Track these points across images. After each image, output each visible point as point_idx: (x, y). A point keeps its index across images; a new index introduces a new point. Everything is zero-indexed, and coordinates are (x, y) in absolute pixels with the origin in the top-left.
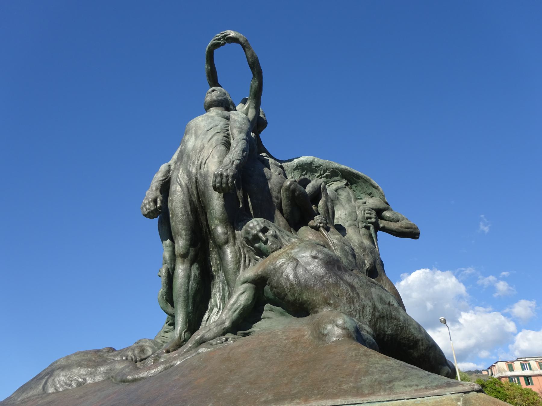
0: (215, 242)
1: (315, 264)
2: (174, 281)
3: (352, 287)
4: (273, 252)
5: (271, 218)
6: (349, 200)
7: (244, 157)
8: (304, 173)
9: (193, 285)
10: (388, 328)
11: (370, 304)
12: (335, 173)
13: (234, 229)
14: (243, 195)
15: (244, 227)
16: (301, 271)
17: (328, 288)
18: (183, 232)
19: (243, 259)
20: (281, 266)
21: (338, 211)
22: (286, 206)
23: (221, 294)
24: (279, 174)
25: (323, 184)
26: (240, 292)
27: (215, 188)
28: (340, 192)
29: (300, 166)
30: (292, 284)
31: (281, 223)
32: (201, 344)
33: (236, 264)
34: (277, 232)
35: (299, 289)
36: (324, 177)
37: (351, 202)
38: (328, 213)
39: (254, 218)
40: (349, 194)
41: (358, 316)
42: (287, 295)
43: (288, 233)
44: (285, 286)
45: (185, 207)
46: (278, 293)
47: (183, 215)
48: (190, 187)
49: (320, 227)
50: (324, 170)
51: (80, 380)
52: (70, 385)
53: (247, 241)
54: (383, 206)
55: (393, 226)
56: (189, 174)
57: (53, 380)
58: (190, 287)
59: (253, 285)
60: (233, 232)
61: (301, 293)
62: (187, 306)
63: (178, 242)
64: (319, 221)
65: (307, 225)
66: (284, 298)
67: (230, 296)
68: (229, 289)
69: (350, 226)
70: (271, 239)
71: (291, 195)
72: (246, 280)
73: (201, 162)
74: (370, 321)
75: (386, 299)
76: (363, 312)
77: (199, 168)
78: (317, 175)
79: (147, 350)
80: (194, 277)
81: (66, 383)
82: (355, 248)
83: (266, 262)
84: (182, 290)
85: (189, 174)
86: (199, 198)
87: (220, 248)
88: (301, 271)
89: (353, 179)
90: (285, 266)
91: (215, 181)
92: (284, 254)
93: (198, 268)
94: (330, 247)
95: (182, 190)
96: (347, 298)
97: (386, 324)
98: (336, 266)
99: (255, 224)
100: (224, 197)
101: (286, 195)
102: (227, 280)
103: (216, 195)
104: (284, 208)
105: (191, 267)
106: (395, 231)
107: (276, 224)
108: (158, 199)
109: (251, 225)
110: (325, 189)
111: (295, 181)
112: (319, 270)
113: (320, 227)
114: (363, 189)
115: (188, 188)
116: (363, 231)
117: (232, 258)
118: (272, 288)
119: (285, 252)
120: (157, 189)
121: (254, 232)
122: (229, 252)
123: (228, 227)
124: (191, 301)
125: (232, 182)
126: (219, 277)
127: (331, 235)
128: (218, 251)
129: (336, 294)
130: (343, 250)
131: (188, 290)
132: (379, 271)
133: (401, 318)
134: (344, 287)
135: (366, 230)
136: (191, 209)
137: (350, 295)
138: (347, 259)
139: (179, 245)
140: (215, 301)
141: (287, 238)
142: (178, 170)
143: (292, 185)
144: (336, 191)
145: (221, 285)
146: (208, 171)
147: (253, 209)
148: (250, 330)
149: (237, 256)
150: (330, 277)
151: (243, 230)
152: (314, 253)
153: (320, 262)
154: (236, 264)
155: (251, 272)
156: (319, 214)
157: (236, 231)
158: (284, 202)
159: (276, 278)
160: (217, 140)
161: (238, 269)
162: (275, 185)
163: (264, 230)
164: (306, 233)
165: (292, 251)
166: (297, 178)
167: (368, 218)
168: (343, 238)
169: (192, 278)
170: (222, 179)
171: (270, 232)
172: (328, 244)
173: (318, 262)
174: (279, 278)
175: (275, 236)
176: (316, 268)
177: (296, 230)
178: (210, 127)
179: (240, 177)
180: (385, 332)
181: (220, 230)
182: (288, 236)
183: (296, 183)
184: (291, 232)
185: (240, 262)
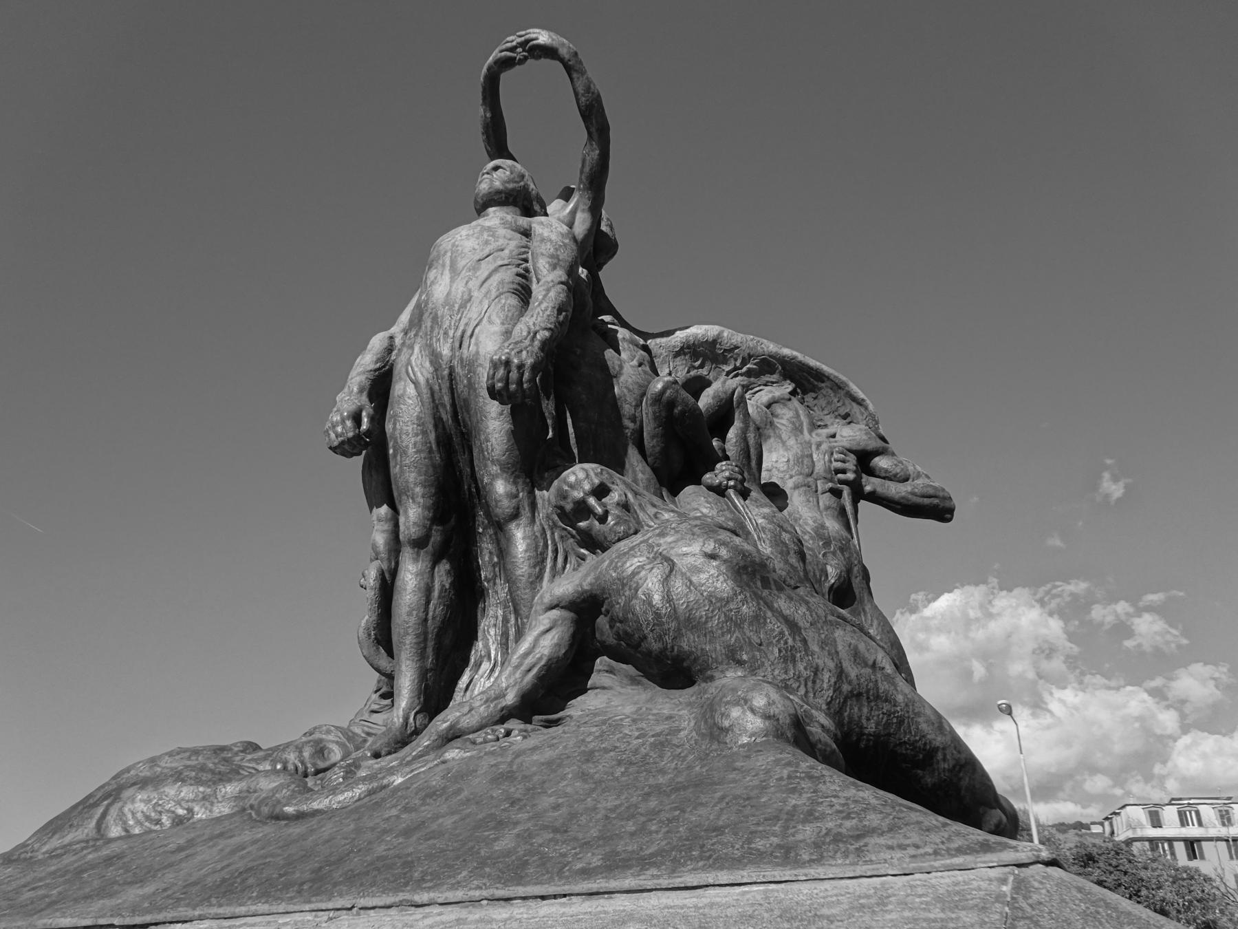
0: (488, 514)
1: (712, 572)
2: (395, 598)
4: (619, 540)
5: (617, 463)
6: (797, 430)
7: (561, 324)
8: (697, 364)
10: (868, 719)
11: (831, 665)
12: (767, 367)
14: (557, 409)
15: (556, 483)
16: (678, 586)
18: (418, 490)
20: (634, 574)
21: (770, 452)
22: (653, 437)
23: (499, 632)
24: (640, 365)
25: (739, 389)
26: (542, 628)
27: (493, 393)
28: (778, 409)
29: (689, 347)
30: (657, 615)
31: (640, 476)
32: (450, 740)
33: (535, 567)
34: (630, 496)
35: (673, 625)
36: (742, 375)
37: (802, 432)
38: (748, 457)
39: (580, 462)
40: (798, 416)
41: (802, 691)
42: (645, 637)
43: (656, 500)
44: (642, 619)
45: (424, 433)
46: (626, 632)
47: (418, 452)
48: (436, 387)
49: (727, 487)
51: (181, 812)
52: (158, 822)
53: (562, 513)
54: (875, 444)
55: (895, 490)
56: (435, 357)
57: (121, 809)
58: (431, 614)
59: (572, 614)
60: (531, 493)
61: (678, 635)
62: (422, 655)
63: (406, 512)
64: (727, 474)
65: (698, 482)
66: (639, 645)
67: (520, 635)
68: (516, 619)
69: (796, 487)
70: (614, 511)
71: (663, 414)
73: (464, 332)
74: (828, 704)
75: (867, 655)
76: (814, 682)
77: (457, 345)
78: (727, 368)
79: (331, 751)
80: (441, 592)
81: (148, 818)
82: (806, 537)
84: (413, 620)
85: (435, 357)
87: (500, 527)
88: (678, 586)
89: (809, 381)
90: (643, 573)
93: (448, 573)
95: (419, 394)
96: (780, 651)
97: (865, 710)
99: (580, 477)
100: (513, 413)
101: (654, 413)
102: (513, 600)
105: (433, 568)
106: (897, 503)
107: (629, 480)
108: (364, 414)
109: (572, 479)
110: (742, 400)
111: (676, 382)
112: (719, 585)
114: (829, 403)
116: (826, 499)
117: (526, 551)
118: (612, 622)
120: (361, 391)
121: (578, 494)
122: (520, 538)
123: (520, 481)
124: (431, 644)
126: (496, 592)
127: (751, 507)
128: (496, 534)
129: (755, 640)
130: (777, 542)
131: (426, 620)
132: (857, 591)
133: (900, 698)
134: (774, 625)
135: (834, 499)
136: (437, 437)
137: (786, 643)
138: (786, 562)
139: (407, 517)
140: (487, 646)
141: (651, 511)
142: (411, 347)
144: (769, 406)
145: (500, 612)
146: (477, 353)
147: (577, 442)
148: (561, 714)
149: (537, 547)
150: (744, 601)
151: (552, 489)
152: (710, 547)
153: (723, 568)
154: (535, 567)
155: (567, 585)
156: (727, 458)
157: (537, 492)
158: (648, 429)
159: (622, 601)
160: (502, 282)
161: (540, 577)
162: (629, 390)
163: (601, 491)
164: (696, 500)
165: (662, 541)
166: (682, 374)
167: (838, 471)
168: (779, 515)
169: (436, 594)
171: (614, 497)
172: (743, 527)
173: (718, 567)
175: (626, 506)
176: (714, 580)
177: (674, 492)
178: (487, 251)
179: (551, 369)
180: (862, 727)
181: (501, 487)
182: (654, 506)
184: (662, 497)
185: (544, 560)
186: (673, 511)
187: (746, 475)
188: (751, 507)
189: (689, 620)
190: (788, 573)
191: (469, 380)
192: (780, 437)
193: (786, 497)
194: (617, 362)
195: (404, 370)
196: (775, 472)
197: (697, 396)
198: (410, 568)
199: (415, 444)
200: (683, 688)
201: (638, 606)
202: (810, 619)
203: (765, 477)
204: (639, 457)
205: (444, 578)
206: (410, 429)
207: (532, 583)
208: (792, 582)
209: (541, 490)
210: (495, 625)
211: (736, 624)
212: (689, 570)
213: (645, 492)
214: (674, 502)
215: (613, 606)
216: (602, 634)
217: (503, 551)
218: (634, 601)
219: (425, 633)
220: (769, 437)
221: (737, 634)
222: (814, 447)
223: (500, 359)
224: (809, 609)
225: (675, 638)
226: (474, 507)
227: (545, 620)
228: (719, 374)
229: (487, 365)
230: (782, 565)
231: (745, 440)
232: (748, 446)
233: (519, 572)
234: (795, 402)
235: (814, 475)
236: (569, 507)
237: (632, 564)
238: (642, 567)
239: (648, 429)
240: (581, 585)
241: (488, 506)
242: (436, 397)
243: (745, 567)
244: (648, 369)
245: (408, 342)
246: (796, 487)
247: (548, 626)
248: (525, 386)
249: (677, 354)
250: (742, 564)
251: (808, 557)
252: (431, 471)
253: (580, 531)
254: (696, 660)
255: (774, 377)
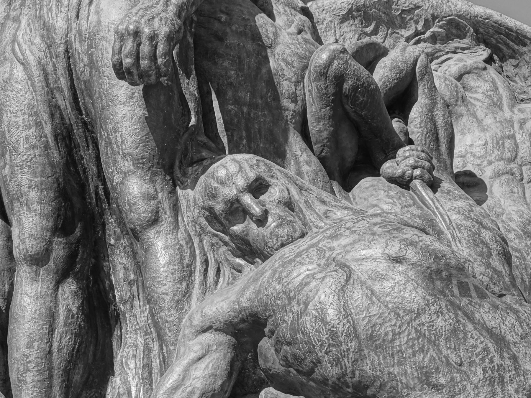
0: (121, 222)
1: (398, 278)
2: (11, 327)
3: (500, 341)
4: (283, 245)
5: (277, 154)
6: (496, 105)
8: (369, 29)
9: (63, 340)
12: (455, 28)
13: (175, 185)
14: (200, 88)
15: (202, 178)
16: (357, 297)
17: (434, 343)
18: (33, 195)
19: (199, 266)
20: (303, 285)
21: (463, 133)
22: (318, 120)
23: (140, 364)
24: (300, 32)
25: (423, 58)
26: (192, 356)
27: (121, 72)
28: (471, 81)
30: (333, 334)
31: (305, 168)
33: (180, 282)
34: (294, 191)
35: (353, 345)
36: (425, 41)
37: (500, 108)
38: (437, 140)
39: (231, 153)
40: (495, 88)
42: (319, 362)
43: (325, 195)
44: (314, 339)
45: (39, 125)
46: (295, 357)
48: (50, 68)
50: (426, 21)
53: (212, 217)
56: (47, 31)
58: (56, 345)
59: (229, 338)
60: (173, 192)
61: (359, 357)
63: (19, 221)
64: (411, 161)
65: (375, 172)
66: (312, 371)
67: (165, 365)
68: (161, 347)
69: (497, 175)
70: (275, 211)
71: (331, 90)
72: (208, 324)
77: (73, 14)
78: (407, 33)
80: (67, 318)
82: (511, 236)
83: (263, 272)
84: (34, 353)
85: (47, 31)
86: (75, 99)
87: (135, 235)
88: (357, 297)
89: (507, 45)
90: (314, 283)
91: (120, 53)
92: (313, 252)
93: (76, 294)
94: (439, 234)
95: (30, 77)
96: (485, 372)
98: (455, 282)
99: (232, 171)
100: (147, 94)
101: (319, 90)
102: (156, 324)
103: (122, 90)
104: (314, 127)
105: (56, 289)
107: (291, 171)
109: (222, 173)
110: (427, 71)
111: (344, 51)
112: (407, 294)
113: (412, 178)
115: (44, 70)
117: (169, 264)
118: (278, 344)
119: (316, 245)
121: (230, 192)
122: (161, 248)
124: (57, 381)
125: (169, 53)
126: (135, 316)
127: (442, 201)
128: (131, 245)
129: (454, 358)
130: (476, 241)
131: (50, 352)
134: (477, 340)
136: (54, 129)
137: (492, 361)
138: (488, 265)
139: (21, 229)
140: (125, 382)
141: (320, 208)
142: (17, 20)
143: (336, 62)
144: (459, 78)
145: (140, 340)
146: (99, 23)
147: (227, 129)
149: (182, 258)
150: (439, 313)
151: (199, 187)
152: (394, 249)
153: (411, 273)
154: (180, 282)
155: (223, 301)
156: (410, 142)
157: (179, 191)
158: (314, 110)
159: (289, 318)
161: (187, 294)
162: (288, 64)
163: (258, 187)
164: (370, 190)
165: (335, 244)
166: (351, 42)
168: (477, 209)
169: (61, 320)
170: (139, 45)
171: (274, 194)
172: (432, 224)
173: (405, 273)
174: (299, 316)
175: (289, 205)
176: (403, 288)
177: (348, 186)
179: (191, 40)
182: (324, 203)
183: (346, 56)
184: (333, 192)
185: (191, 273)
186: (346, 208)
187: (434, 161)
188: (442, 201)
189: (371, 338)
190: (491, 279)
191: (90, 56)
192: (474, 115)
193: (485, 188)
194: (271, 29)
195: (9, 48)
196: (469, 158)
197: (370, 66)
198: (28, 290)
199: (27, 139)
200: (284, 393)
201: (308, 322)
202: (520, 331)
203: (458, 165)
204: (304, 145)
205: (71, 301)
206: (20, 120)
207: (178, 302)
208: (496, 289)
209: (185, 188)
210: (135, 356)
211: (430, 341)
212: (370, 277)
213: (312, 187)
214: (348, 199)
215: (278, 325)
216: (266, 360)
217: (140, 267)
218: (304, 318)
219: (50, 369)
220: (461, 115)
221: (431, 353)
222: (516, 126)
223: (127, 29)
224: (518, 319)
225: (356, 360)
226: (102, 214)
227: (195, 346)
228: (397, 40)
229: (112, 37)
230: (482, 269)
231: (432, 120)
232: (436, 127)
233: (162, 289)
234: (492, 72)
235: (518, 160)
236: (219, 207)
237: (300, 273)
238: (312, 276)
239: (314, 110)
240: (238, 302)
241: (120, 211)
242: (51, 79)
243: (438, 272)
244: (309, 36)
245: (13, 14)
246: (497, 175)
247: (199, 353)
248: (160, 61)
249: (344, 19)
250: (434, 267)
251: (514, 259)
252: (48, 170)
253: (234, 237)
254: (382, 387)
255: (465, 42)
